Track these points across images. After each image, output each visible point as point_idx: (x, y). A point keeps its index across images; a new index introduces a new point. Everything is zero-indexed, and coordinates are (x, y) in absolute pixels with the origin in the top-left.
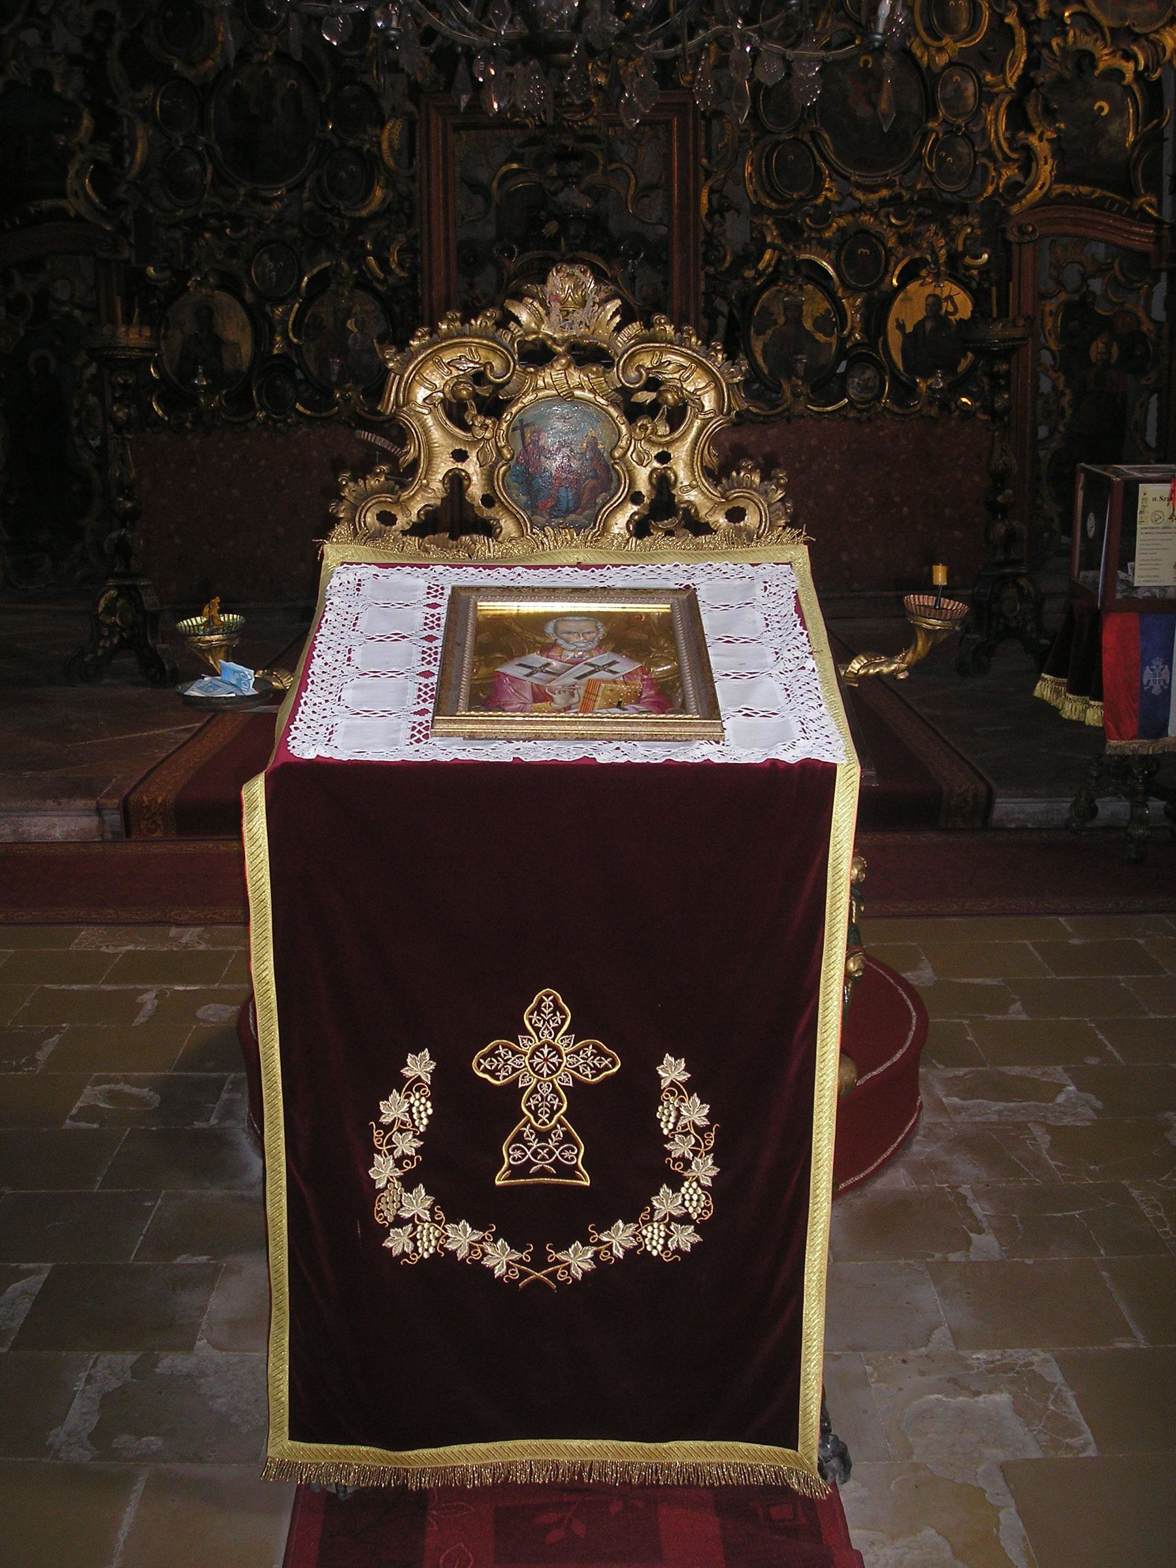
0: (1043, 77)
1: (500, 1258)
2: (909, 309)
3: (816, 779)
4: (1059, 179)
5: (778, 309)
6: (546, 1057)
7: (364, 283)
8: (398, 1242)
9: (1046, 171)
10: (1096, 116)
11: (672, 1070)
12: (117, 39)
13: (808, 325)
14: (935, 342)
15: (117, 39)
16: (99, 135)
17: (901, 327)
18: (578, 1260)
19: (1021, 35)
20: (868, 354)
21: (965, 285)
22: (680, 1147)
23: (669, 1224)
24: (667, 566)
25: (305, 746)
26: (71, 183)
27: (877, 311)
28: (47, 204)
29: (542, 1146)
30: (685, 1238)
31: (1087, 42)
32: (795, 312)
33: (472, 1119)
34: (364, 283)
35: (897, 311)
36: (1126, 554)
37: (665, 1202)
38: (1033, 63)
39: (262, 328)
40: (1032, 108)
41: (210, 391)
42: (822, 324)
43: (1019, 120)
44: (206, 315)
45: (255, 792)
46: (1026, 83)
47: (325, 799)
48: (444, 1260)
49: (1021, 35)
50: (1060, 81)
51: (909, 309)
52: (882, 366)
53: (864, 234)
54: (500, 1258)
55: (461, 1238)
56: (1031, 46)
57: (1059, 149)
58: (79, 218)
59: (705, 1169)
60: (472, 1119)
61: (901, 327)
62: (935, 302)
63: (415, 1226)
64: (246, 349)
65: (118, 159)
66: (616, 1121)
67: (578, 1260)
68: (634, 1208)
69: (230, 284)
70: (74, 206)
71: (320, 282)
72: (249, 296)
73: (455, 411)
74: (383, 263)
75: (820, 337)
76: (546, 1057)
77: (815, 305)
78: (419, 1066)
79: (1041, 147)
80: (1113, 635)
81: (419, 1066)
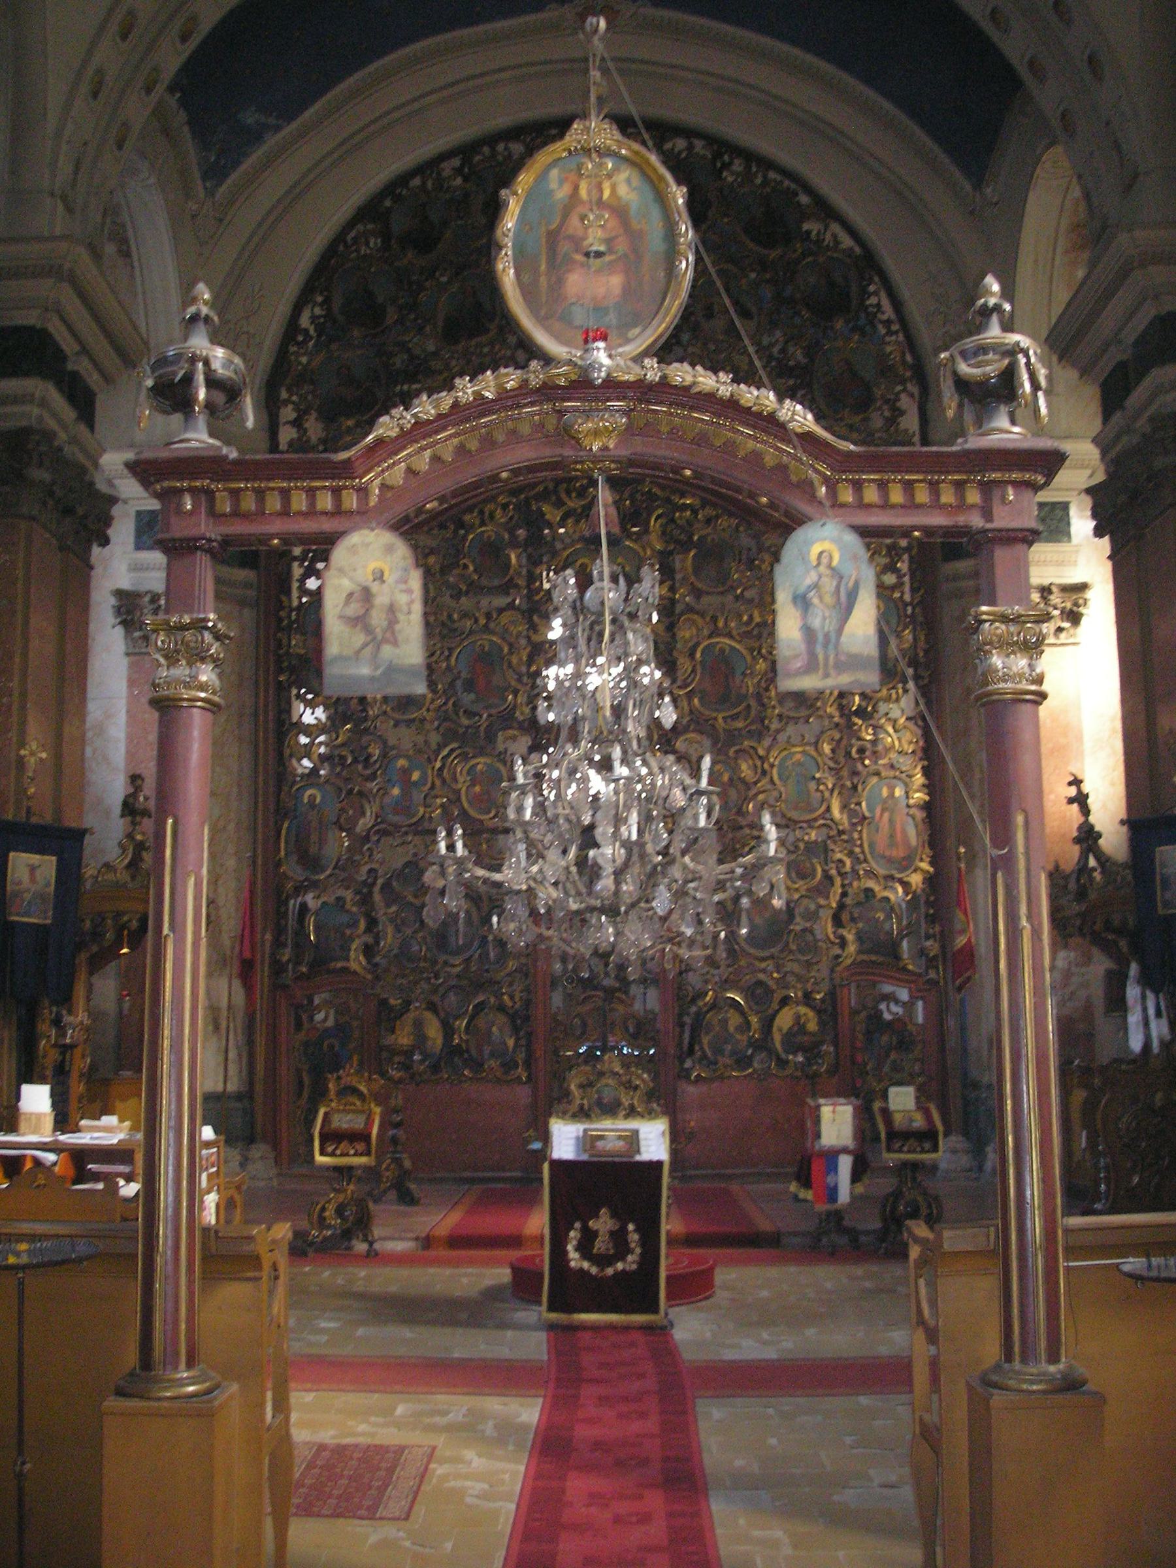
0: (848, 901)
1: (594, 1270)
2: (784, 1020)
3: (659, 1164)
4: (860, 952)
5: (715, 1022)
6: (603, 1223)
7: (501, 1008)
8: (573, 1264)
9: (852, 948)
10: (877, 920)
11: (631, 1227)
12: (380, 882)
13: (731, 1029)
14: (795, 1037)
15: (380, 882)
16: (368, 930)
17: (780, 1030)
18: (610, 1271)
19: (838, 881)
20: (763, 1045)
21: (813, 1008)
22: (633, 1245)
23: (630, 1263)
24: (632, 1124)
25: (556, 1155)
26: (352, 954)
27: (768, 1024)
28: (340, 965)
29: (601, 1245)
30: (634, 1267)
31: (871, 884)
32: (725, 1021)
33: (588, 1237)
34: (501, 1008)
35: (778, 1022)
36: (818, 1136)
37: (630, 1258)
38: (844, 894)
39: (448, 1030)
40: (845, 917)
41: (422, 1062)
42: (739, 1029)
43: (837, 921)
44: (418, 1025)
45: (546, 1166)
46: (841, 906)
47: (560, 1166)
48: (581, 1270)
49: (838, 881)
50: (859, 904)
51: (784, 1020)
52: (771, 1051)
53: (760, 983)
54: (594, 1270)
55: (586, 1265)
56: (843, 886)
57: (859, 938)
58: (355, 973)
59: (638, 1250)
60: (588, 1237)
61: (780, 1030)
62: (798, 1017)
63: (574, 1259)
64: (439, 1042)
65: (378, 943)
66: (619, 1237)
67: (610, 1271)
68: (623, 1258)
69: (432, 1007)
70: (354, 966)
71: (479, 1008)
72: (442, 1015)
73: (581, 1086)
74: (512, 998)
75: (738, 1036)
76: (603, 1223)
77: (734, 1020)
78: (577, 1225)
79: (850, 937)
80: (816, 1166)
81: (577, 1225)
